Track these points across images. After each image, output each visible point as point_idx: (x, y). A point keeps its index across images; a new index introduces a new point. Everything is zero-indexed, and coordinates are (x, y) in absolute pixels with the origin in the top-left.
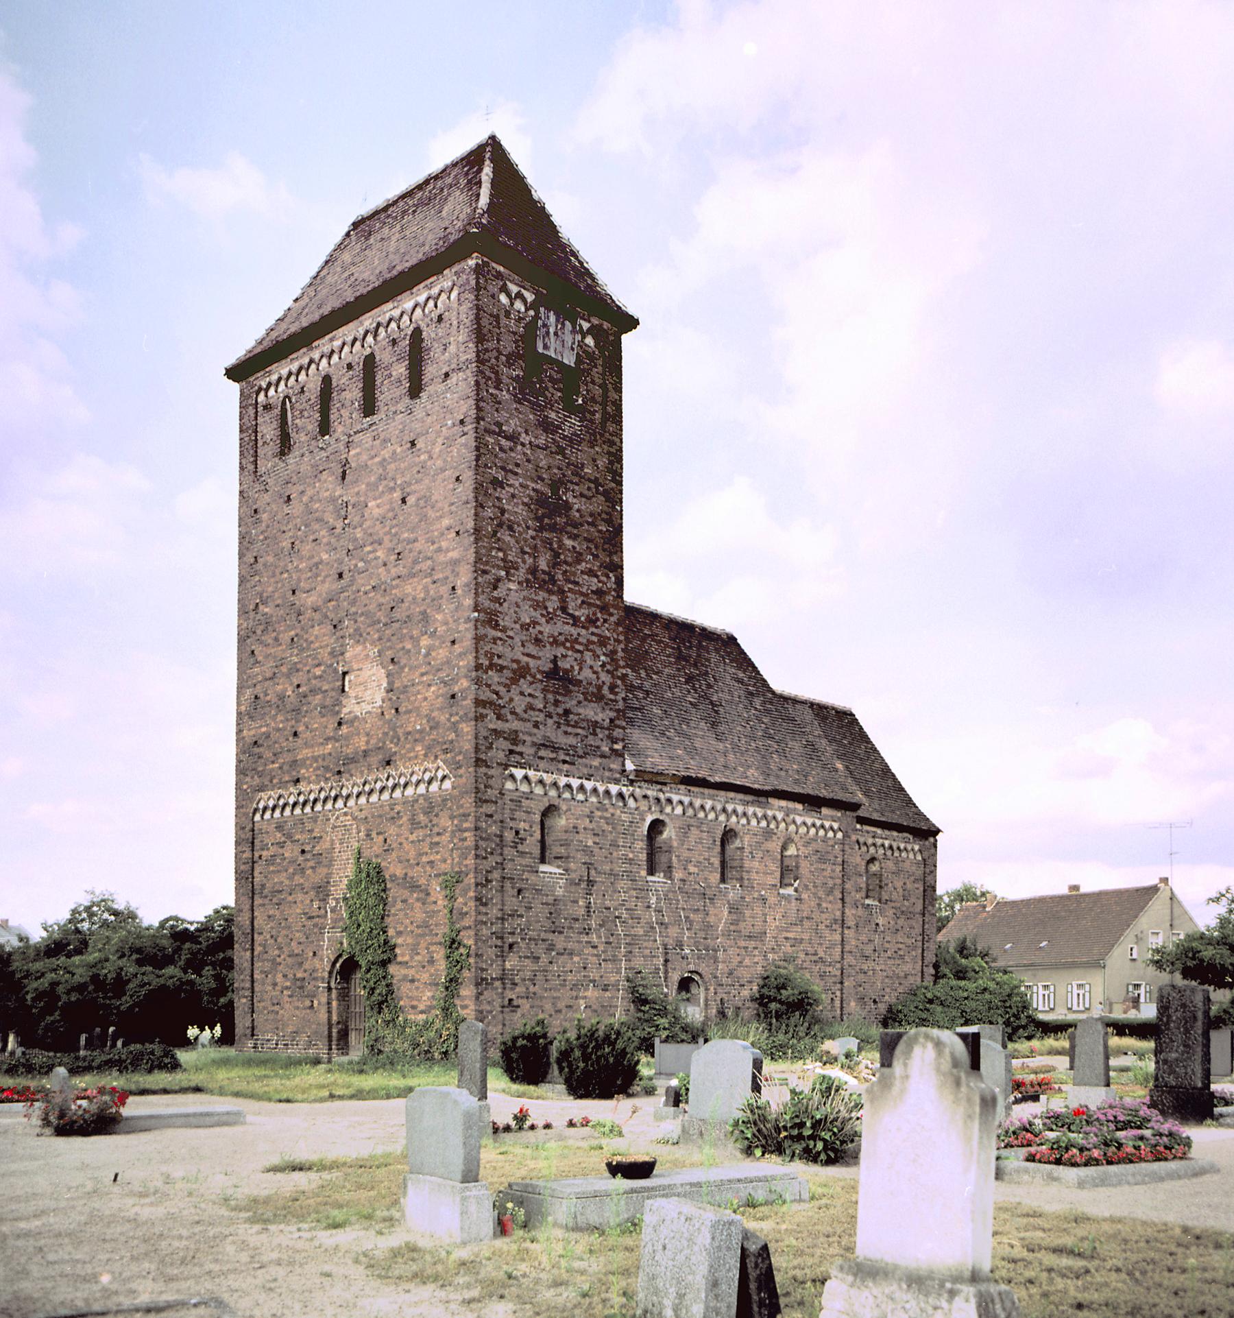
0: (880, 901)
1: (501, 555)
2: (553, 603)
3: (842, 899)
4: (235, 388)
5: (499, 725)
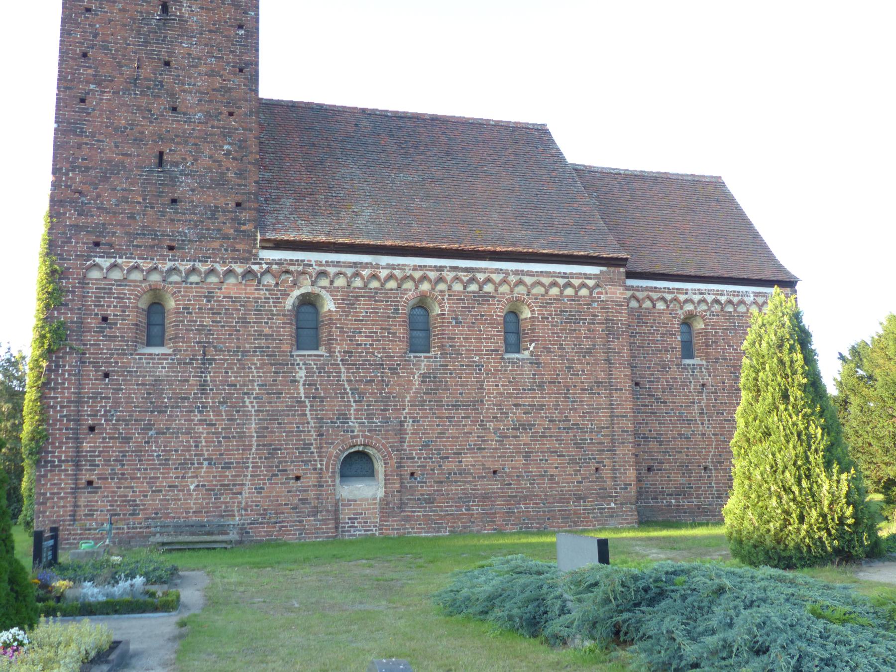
0: (707, 360)
1: (91, 72)
2: (159, 106)
3: (608, 361)
5: (82, 221)
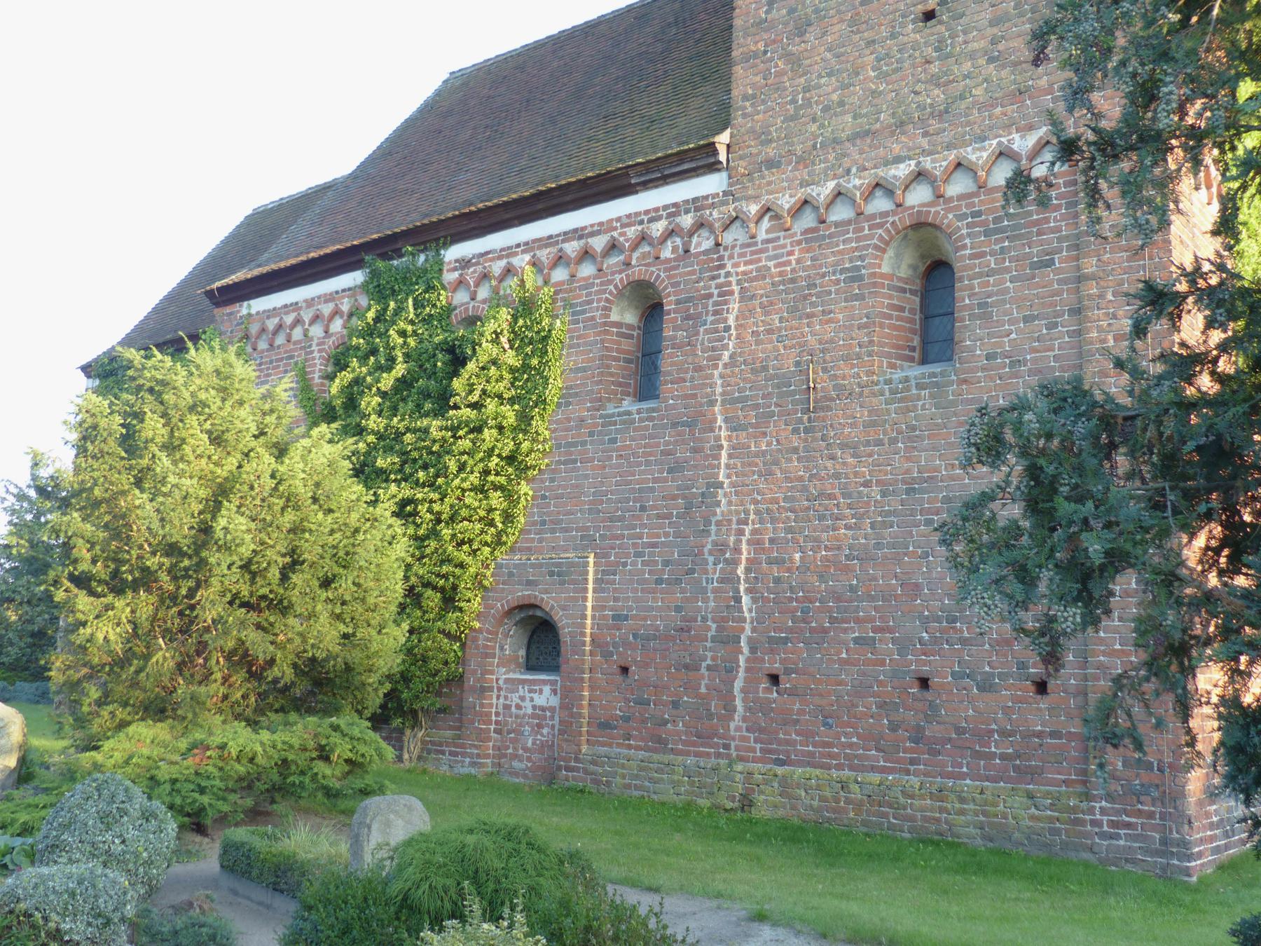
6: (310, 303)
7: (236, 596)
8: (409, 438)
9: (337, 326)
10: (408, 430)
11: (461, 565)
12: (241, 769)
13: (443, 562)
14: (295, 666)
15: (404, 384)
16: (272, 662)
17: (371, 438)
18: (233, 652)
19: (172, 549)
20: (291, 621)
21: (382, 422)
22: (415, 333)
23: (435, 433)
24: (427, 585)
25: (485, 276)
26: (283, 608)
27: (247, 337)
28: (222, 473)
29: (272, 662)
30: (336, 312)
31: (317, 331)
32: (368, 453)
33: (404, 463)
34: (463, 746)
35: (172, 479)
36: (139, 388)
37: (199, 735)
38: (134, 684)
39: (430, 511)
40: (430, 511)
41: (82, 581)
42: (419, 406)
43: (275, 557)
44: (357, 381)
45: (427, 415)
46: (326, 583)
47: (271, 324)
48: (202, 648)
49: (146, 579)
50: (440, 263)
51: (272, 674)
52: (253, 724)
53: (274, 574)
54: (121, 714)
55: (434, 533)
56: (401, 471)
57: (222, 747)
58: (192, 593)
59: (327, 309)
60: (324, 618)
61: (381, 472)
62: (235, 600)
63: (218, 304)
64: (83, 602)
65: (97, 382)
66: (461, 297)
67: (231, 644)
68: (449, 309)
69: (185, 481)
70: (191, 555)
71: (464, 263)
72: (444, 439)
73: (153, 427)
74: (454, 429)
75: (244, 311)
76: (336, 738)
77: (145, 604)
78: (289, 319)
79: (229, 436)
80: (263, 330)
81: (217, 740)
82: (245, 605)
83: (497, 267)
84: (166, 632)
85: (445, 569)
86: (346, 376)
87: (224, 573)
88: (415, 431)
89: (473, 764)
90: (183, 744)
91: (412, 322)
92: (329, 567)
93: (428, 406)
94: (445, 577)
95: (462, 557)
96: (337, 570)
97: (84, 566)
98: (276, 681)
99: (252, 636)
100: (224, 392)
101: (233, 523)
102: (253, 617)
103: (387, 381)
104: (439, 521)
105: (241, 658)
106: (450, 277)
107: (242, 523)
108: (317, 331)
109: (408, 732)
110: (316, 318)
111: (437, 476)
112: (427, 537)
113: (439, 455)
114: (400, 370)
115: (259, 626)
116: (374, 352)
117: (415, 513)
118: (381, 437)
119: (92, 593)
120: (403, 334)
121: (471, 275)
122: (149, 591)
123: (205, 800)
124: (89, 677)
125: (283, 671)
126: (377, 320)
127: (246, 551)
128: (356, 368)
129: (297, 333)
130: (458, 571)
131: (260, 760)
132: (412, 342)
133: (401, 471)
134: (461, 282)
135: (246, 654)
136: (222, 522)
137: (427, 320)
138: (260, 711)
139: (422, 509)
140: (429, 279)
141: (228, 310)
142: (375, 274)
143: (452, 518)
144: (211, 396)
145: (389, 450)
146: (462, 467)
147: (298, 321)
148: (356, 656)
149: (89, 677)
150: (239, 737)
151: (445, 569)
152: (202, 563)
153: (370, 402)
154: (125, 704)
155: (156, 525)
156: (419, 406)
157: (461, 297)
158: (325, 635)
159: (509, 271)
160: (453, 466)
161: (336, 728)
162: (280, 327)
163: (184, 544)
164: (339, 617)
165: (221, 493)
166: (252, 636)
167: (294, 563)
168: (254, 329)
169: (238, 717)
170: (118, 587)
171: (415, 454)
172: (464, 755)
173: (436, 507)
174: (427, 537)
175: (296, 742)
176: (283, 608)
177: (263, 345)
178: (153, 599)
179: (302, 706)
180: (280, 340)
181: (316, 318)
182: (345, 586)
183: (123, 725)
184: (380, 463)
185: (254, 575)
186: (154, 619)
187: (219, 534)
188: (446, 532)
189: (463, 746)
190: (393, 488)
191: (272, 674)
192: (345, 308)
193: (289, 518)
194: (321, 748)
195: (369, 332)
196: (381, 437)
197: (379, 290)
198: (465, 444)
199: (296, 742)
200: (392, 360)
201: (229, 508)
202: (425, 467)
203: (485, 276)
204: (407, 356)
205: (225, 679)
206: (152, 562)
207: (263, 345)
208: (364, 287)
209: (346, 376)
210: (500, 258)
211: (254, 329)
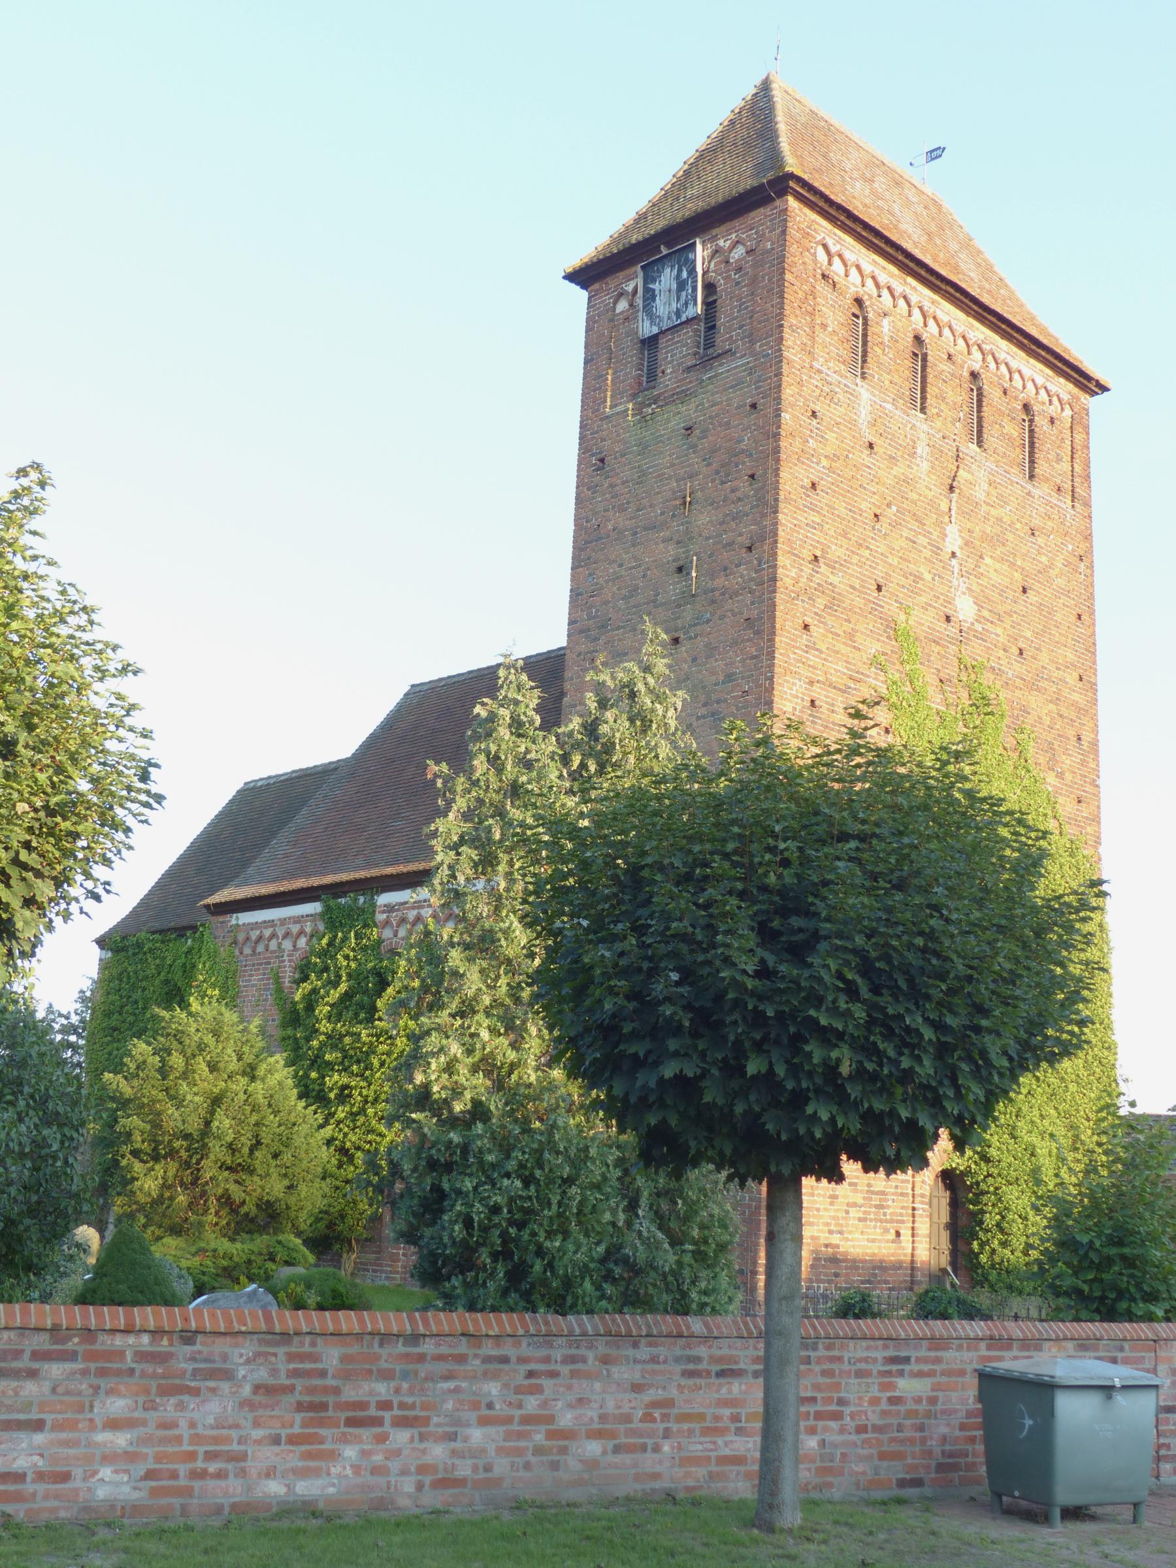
4: (579, 296)
6: (283, 922)
7: (223, 1163)
8: (347, 1040)
9: (302, 942)
10: (348, 1033)
11: (380, 1135)
12: (225, 1263)
13: (369, 1132)
14: (257, 1205)
15: (347, 996)
16: (243, 1203)
17: (322, 1038)
18: (222, 1197)
19: (187, 1136)
20: (256, 1178)
21: (330, 1026)
22: (355, 959)
23: (364, 1038)
24: (358, 1148)
25: (403, 920)
26: (251, 1171)
27: (235, 942)
28: (216, 1090)
29: (243, 1203)
30: (302, 932)
31: (287, 945)
32: (320, 1049)
33: (345, 1057)
34: (381, 1265)
35: (189, 1097)
36: (168, 1035)
37: (202, 1245)
38: (164, 1215)
39: (360, 1094)
40: (360, 1094)
41: (135, 1153)
42: (356, 1015)
43: (246, 1142)
44: (314, 991)
45: (360, 1023)
46: (275, 1156)
47: (254, 935)
48: (204, 1193)
49: (172, 1153)
50: (374, 905)
51: (243, 1210)
52: (232, 1240)
53: (246, 1150)
54: (157, 1232)
55: (362, 1111)
56: (342, 1063)
57: (215, 1250)
58: (198, 1163)
59: (295, 929)
60: (275, 1176)
61: (328, 1063)
62: (223, 1167)
63: (213, 914)
64: (138, 1167)
65: (109, 954)
66: (387, 933)
67: (220, 1191)
68: (380, 942)
69: (194, 1097)
70: (199, 1141)
71: (390, 908)
72: (371, 1043)
73: (177, 1060)
74: (378, 1036)
75: (234, 922)
76: (279, 1248)
77: (173, 1167)
78: (267, 933)
79: (221, 1065)
80: (248, 939)
81: (213, 1245)
82: (228, 1168)
83: (412, 915)
84: (182, 1184)
85: (370, 1137)
86: (307, 987)
87: (217, 1150)
88: (352, 1034)
89: (387, 1278)
90: (193, 1249)
91: (353, 950)
92: (276, 1146)
93: (362, 1016)
94: (370, 1142)
95: (383, 1129)
96: (282, 1148)
97: (137, 1146)
98: (247, 1214)
99: (233, 1188)
100: (216, 1034)
101: (223, 1123)
102: (233, 1177)
103: (335, 995)
104: (366, 1102)
105: (226, 1200)
106: (380, 917)
107: (227, 1122)
108: (287, 945)
109: (345, 1256)
110: (287, 935)
111: (366, 1069)
112: (358, 1114)
113: (367, 1054)
114: (343, 987)
115: (237, 1182)
116: (326, 969)
117: (350, 1096)
118: (329, 1037)
119: (142, 1161)
120: (347, 957)
121: (394, 918)
122: (173, 1159)
123: (206, 1278)
124: (138, 1210)
125: (250, 1208)
126: (330, 944)
127: (229, 1139)
128: (314, 981)
129: (273, 945)
130: (378, 1139)
131: (236, 1259)
132: (353, 965)
133: (342, 1063)
134: (387, 923)
135: (229, 1198)
136: (216, 1123)
137: (364, 949)
138: (237, 1233)
139: (355, 1093)
140: (365, 917)
141: (221, 919)
142: (328, 909)
143: (376, 1100)
144: (209, 1039)
145: (334, 1047)
146: (382, 1064)
147: (273, 936)
148: (292, 1200)
149: (138, 1210)
150: (224, 1245)
151: (370, 1137)
152: (205, 1146)
153: (322, 1010)
154: (160, 1227)
155: (180, 1124)
156: (356, 1015)
157: (387, 933)
158: (276, 1188)
159: (418, 919)
160: (376, 1062)
161: (279, 1242)
162: (260, 938)
163: (196, 1135)
164: (285, 1175)
165: (216, 1101)
166: (233, 1188)
167: (258, 1144)
168: (241, 937)
169: (224, 1236)
170: (156, 1158)
171: (352, 1052)
172: (382, 1272)
173: (365, 1092)
174: (358, 1114)
175: (256, 1250)
176: (251, 1171)
177: (247, 951)
178: (177, 1165)
179: (263, 1229)
180: (260, 948)
181: (287, 935)
182: (287, 1157)
183: (159, 1238)
184: (327, 1057)
185: (234, 1151)
186: (176, 1176)
187: (214, 1130)
188: (370, 1111)
189: (381, 1265)
190: (336, 1077)
191: (243, 1210)
192: (308, 930)
193: (254, 1118)
194: (270, 1254)
195: (323, 954)
196: (329, 1037)
197: (333, 921)
198: (383, 1048)
199: (256, 1250)
200: (339, 977)
201: (220, 1113)
202: (358, 1062)
203: (403, 920)
204: (349, 975)
205: (217, 1213)
206: (177, 1144)
207: (247, 951)
208: (322, 915)
209: (307, 987)
210: (413, 908)
211: (241, 937)
